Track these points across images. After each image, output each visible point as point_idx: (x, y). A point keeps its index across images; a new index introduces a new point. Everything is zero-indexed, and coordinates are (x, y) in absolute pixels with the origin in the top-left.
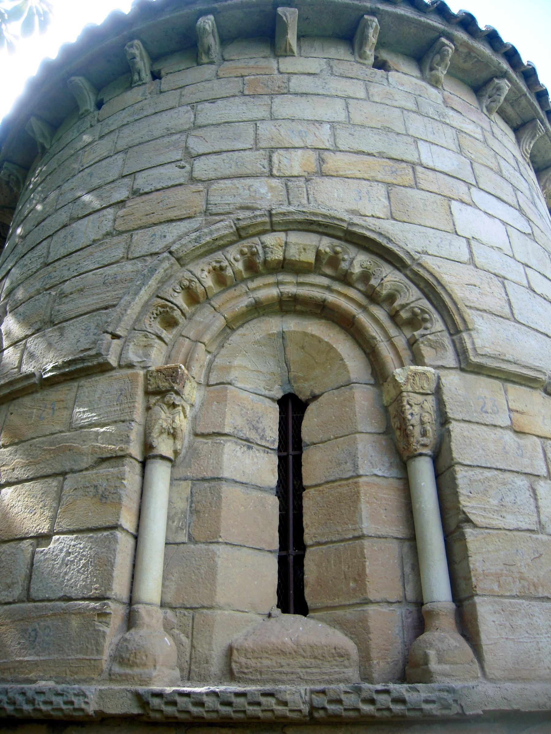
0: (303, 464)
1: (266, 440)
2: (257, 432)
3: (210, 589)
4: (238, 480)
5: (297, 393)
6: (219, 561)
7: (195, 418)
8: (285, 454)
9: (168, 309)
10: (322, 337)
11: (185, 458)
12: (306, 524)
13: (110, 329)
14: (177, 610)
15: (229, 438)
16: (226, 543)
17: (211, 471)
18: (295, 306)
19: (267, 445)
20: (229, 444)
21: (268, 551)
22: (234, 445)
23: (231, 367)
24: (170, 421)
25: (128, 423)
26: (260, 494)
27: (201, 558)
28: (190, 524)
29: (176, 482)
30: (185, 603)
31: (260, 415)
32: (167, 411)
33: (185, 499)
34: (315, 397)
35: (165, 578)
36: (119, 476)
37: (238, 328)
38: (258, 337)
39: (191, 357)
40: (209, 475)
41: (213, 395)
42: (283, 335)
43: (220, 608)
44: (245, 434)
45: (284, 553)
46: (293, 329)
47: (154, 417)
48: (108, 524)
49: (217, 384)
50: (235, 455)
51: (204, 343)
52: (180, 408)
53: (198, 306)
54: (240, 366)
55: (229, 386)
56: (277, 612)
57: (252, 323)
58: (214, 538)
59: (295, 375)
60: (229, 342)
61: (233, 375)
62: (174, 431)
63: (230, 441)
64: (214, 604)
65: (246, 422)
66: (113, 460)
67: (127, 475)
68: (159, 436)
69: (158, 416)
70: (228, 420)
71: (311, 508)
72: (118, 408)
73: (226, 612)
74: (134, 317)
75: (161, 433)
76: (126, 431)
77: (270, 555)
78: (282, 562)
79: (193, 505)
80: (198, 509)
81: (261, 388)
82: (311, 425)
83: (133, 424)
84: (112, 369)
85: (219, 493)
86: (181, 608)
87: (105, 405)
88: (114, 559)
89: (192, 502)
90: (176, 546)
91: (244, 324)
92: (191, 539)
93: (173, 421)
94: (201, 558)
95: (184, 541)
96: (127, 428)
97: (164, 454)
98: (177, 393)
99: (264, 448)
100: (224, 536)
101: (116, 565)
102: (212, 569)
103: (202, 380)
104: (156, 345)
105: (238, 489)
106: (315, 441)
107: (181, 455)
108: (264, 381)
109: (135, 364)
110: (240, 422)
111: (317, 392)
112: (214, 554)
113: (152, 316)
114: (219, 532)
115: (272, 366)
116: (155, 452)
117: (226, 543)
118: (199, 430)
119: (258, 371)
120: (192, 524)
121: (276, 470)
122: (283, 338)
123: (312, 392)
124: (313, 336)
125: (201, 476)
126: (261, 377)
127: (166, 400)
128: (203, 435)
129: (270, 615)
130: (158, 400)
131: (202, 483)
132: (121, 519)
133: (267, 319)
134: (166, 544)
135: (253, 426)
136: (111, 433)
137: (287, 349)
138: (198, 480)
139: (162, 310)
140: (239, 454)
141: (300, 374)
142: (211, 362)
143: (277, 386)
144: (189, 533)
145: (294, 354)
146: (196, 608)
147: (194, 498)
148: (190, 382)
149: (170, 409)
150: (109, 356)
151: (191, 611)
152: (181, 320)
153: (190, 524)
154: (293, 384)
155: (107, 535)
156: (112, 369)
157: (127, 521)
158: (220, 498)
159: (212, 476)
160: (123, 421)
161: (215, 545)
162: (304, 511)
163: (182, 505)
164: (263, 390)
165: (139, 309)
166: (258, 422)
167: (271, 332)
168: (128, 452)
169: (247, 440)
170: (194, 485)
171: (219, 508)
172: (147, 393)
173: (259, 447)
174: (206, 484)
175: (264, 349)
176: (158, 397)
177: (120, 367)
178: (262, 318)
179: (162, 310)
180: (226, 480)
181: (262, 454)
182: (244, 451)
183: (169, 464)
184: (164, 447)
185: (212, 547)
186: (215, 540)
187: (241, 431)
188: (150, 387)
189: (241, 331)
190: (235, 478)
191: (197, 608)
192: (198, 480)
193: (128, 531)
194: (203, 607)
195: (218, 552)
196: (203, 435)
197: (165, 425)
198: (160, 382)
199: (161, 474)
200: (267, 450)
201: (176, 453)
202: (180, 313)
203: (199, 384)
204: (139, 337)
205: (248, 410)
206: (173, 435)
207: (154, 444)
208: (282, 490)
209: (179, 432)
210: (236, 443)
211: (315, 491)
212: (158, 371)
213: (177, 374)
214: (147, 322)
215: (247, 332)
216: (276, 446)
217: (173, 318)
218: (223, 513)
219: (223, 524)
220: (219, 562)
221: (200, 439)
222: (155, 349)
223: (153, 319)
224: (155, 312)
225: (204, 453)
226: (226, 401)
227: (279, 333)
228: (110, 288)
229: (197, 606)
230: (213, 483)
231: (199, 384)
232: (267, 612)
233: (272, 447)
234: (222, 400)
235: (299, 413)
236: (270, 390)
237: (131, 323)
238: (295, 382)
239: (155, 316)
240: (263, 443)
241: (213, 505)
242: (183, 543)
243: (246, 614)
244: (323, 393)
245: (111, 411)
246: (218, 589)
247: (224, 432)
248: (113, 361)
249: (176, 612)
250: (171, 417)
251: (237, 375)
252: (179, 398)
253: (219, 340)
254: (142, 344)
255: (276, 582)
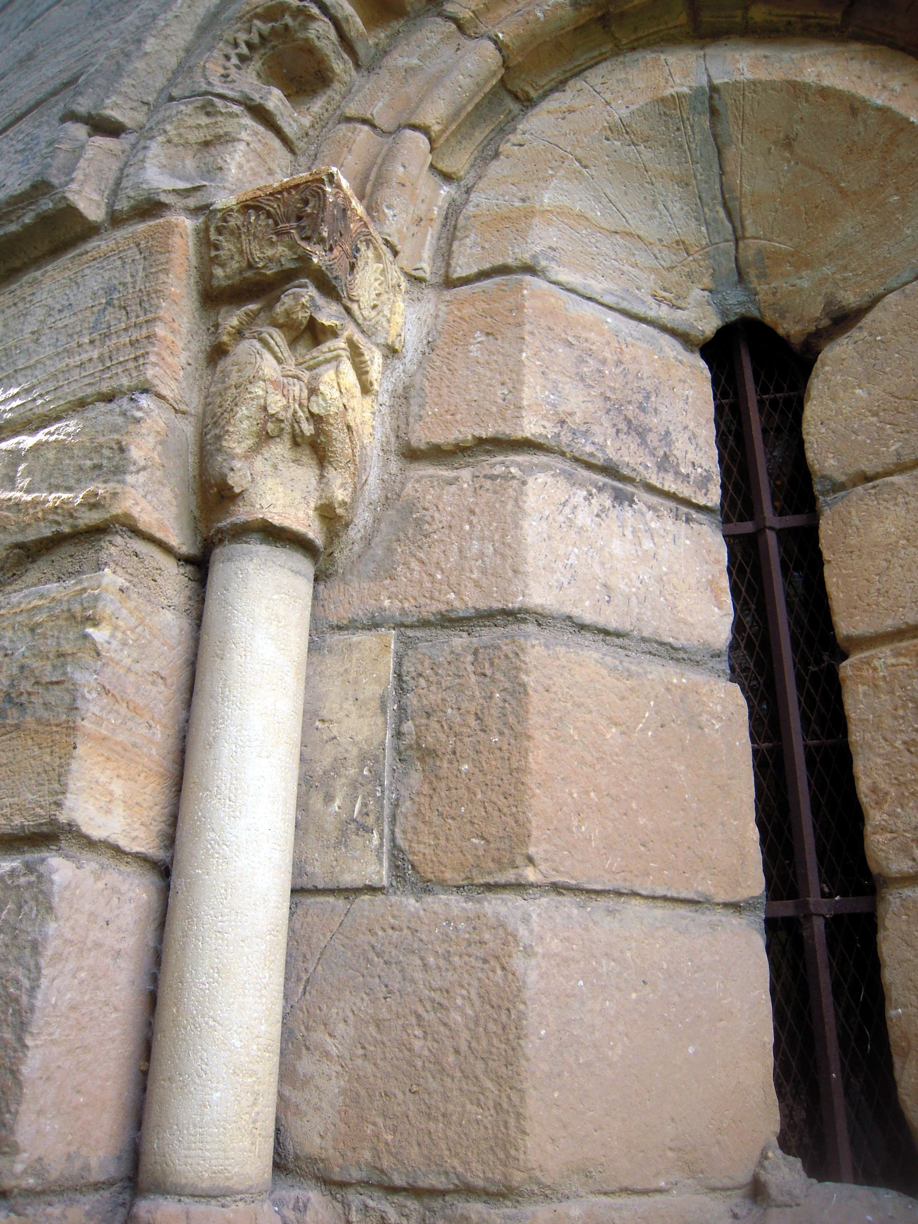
0: (827, 555)
1: (677, 473)
2: (643, 443)
3: (498, 1106)
4: (588, 618)
5: (769, 318)
6: (532, 974)
7: (404, 396)
8: (747, 527)
9: (288, 19)
10: (862, 92)
11: (368, 541)
12: (874, 790)
13: (83, 105)
14: (354, 1198)
15: (542, 458)
16: (557, 888)
17: (477, 584)
18: (746, 9)
19: (685, 491)
20: (542, 478)
21: (726, 905)
22: (562, 483)
23: (529, 214)
24: (298, 390)
25: (125, 403)
26: (678, 677)
27: (447, 956)
28: (396, 805)
29: (335, 639)
30: (386, 1163)
31: (648, 384)
32: (286, 353)
33: (375, 704)
34: (843, 320)
35: (293, 1041)
36: (77, 608)
37: (545, 95)
38: (624, 112)
39: (379, 176)
40: (470, 600)
41: (467, 311)
42: (712, 100)
43: (548, 1193)
44: (602, 448)
45: (786, 909)
46: (749, 76)
47: (234, 378)
48: (17, 821)
49: (483, 275)
50: (570, 522)
51: (425, 130)
52: (341, 343)
53: (397, 25)
54: (562, 212)
55: (528, 278)
56: (786, 1173)
57: (595, 77)
58: (501, 866)
59: (759, 251)
60: (514, 138)
61: (539, 241)
62: (319, 431)
63: (545, 468)
64: (517, 1178)
65: (600, 403)
66: (67, 549)
67: (108, 606)
68: (255, 449)
69: (249, 372)
70: (533, 391)
71: (888, 722)
72: (95, 354)
73: (575, 1210)
74: (172, 62)
75: (265, 438)
76: (115, 429)
77: (734, 921)
78: (785, 942)
79: (408, 726)
80: (429, 741)
81: (644, 294)
82: (838, 414)
83: (145, 401)
84: (90, 230)
85: (514, 669)
86: (366, 1184)
87: (50, 351)
88: (33, 990)
89: (402, 714)
90: (340, 903)
91: (564, 82)
92: (406, 872)
93: (313, 391)
94: (447, 956)
95: (375, 880)
96: (120, 420)
97: (277, 521)
98: (328, 287)
99: (673, 505)
100: (545, 858)
101: (38, 1021)
102: (503, 1012)
103: (426, 268)
104: (244, 135)
105: (591, 657)
106: (868, 466)
107: (355, 533)
108: (653, 270)
109: (164, 198)
110: (577, 402)
111: (850, 298)
112: (510, 938)
113: (233, 53)
114: (524, 838)
115: (675, 217)
116: (242, 514)
117: (557, 888)
118: (421, 437)
119: (630, 234)
120: (406, 806)
121: (725, 583)
122: (714, 112)
123: (829, 303)
124: (825, 92)
125: (436, 607)
126: (642, 258)
127: (279, 309)
128: (438, 454)
129: (757, 1191)
130: (252, 317)
131: (442, 635)
132: (70, 801)
133: (649, 56)
134: (293, 891)
135: (629, 422)
136: (62, 447)
137: (731, 153)
138: (425, 624)
139: (265, 28)
140: (584, 518)
141: (782, 245)
142: (453, 212)
143: (697, 294)
144: (395, 846)
145: (757, 172)
146: (433, 1193)
147: (412, 700)
148: (379, 258)
149: (301, 350)
150: (74, 186)
151: (412, 1205)
152: (340, 65)
153: (396, 805)
154: (754, 283)
155: (12, 873)
156: (90, 230)
157: (109, 800)
158: (519, 692)
159: (482, 605)
160: (109, 398)
161: (508, 896)
162: (856, 735)
163: (360, 727)
164: (651, 300)
165: (189, 36)
166: (642, 409)
167: (669, 91)
168: (117, 510)
169: (609, 470)
170: (407, 644)
171: (519, 735)
172: (213, 298)
173: (654, 500)
174: (459, 640)
175: (647, 155)
176: (253, 307)
177: (116, 220)
178: (629, 57)
179: (265, 28)
180: (541, 618)
181: (669, 524)
182: (603, 510)
183: (306, 566)
184: (280, 492)
185: (496, 906)
186: (510, 876)
187: (585, 434)
188: (219, 272)
189: (555, 102)
190: (575, 612)
191: (443, 1193)
192: (425, 624)
193: (117, 851)
194: (468, 1191)
195: (523, 932)
196: (438, 454)
197: (276, 403)
198: (255, 245)
199: (267, 602)
200: (684, 509)
201: (328, 514)
202: (333, 34)
203: (416, 280)
204: (191, 122)
205: (604, 362)
206: (315, 444)
207: (236, 481)
208: (751, 657)
209: (338, 433)
210: (569, 476)
211: (897, 654)
212: (250, 206)
213: (322, 207)
214: (215, 70)
215: (578, 103)
216: (714, 496)
217: (310, 50)
218: (537, 759)
219: (540, 804)
220: (532, 977)
221: (428, 470)
222: (242, 147)
223: (235, 60)
224: (242, 37)
225: (446, 519)
226: (519, 325)
227: (697, 92)
228: (108, 18)
229: (439, 1182)
230: (487, 635)
231: (416, 280)
232: (744, 1177)
233: (702, 501)
234: (505, 326)
235: (779, 389)
236: (674, 306)
237: (160, 81)
238: (763, 276)
239: (244, 50)
240: (670, 485)
241: (493, 723)
242: (372, 889)
243: (658, 1197)
244: (875, 300)
245: (68, 369)
246: (533, 1105)
247: (519, 435)
248: (90, 203)
249: (346, 1205)
250: (306, 376)
251: (554, 241)
252: (335, 308)
253: (479, 136)
254: (195, 137)
255: (769, 1038)
